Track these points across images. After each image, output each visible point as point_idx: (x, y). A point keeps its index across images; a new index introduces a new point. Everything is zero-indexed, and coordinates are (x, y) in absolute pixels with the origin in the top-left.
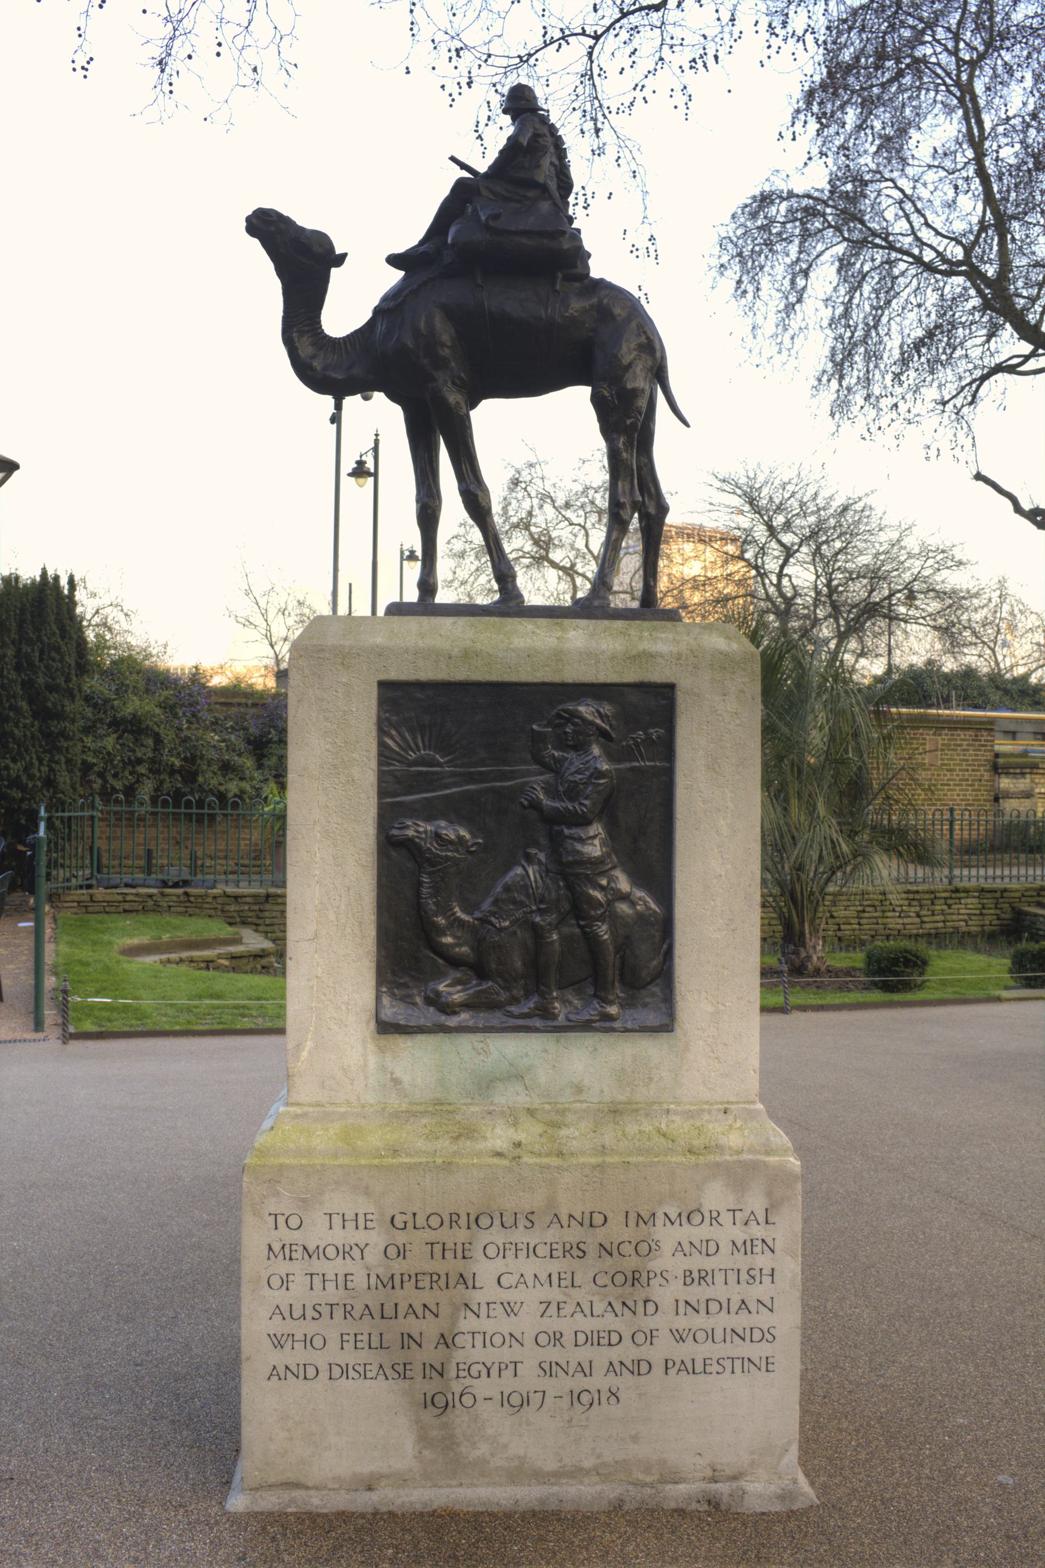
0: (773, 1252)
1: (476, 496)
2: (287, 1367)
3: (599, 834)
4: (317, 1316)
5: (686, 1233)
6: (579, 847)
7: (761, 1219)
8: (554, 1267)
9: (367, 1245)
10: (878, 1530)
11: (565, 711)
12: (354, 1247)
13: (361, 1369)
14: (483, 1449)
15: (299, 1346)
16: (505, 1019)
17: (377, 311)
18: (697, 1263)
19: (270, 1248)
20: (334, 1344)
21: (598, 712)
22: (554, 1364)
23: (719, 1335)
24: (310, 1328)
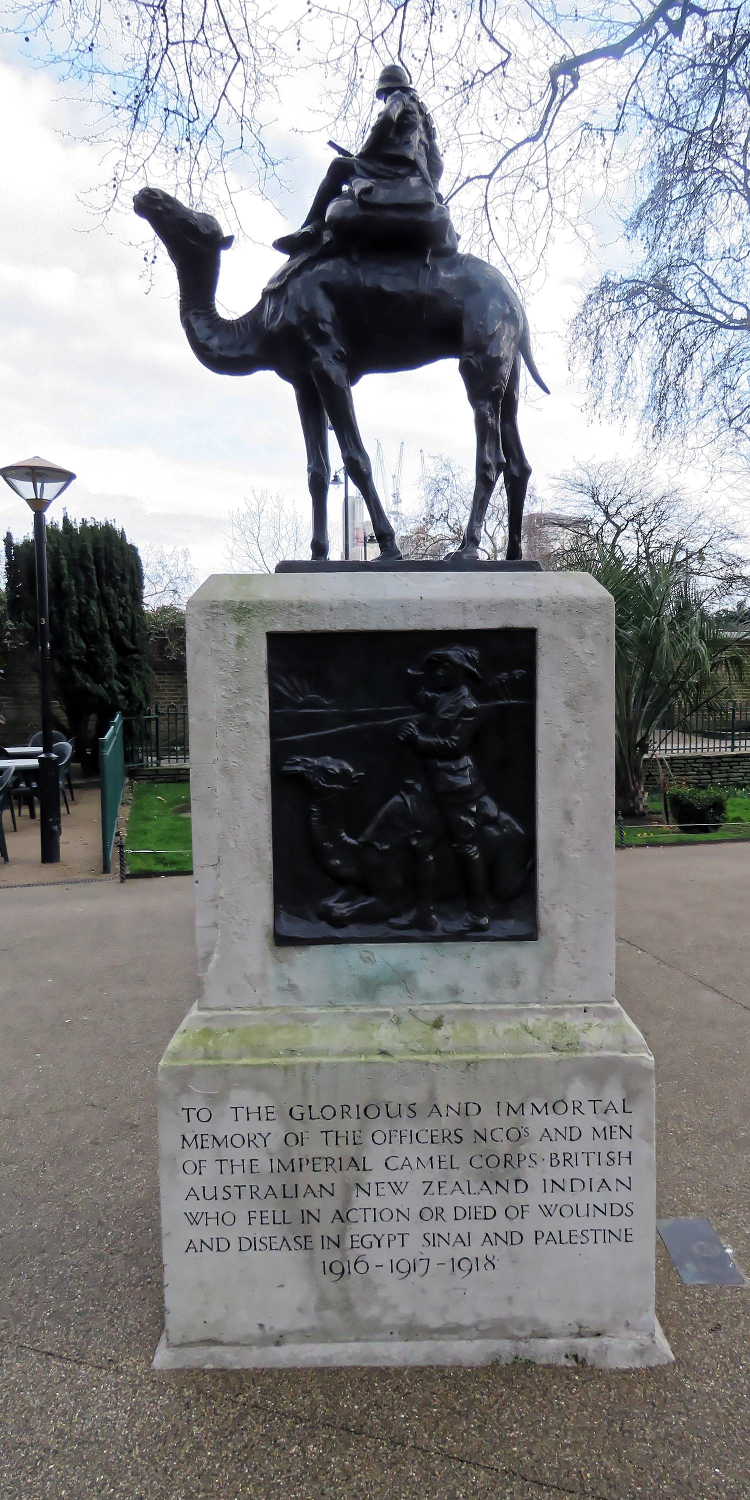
0: (630, 1137)
1: (357, 462)
2: (202, 1241)
3: (469, 765)
4: (227, 1196)
5: (551, 1121)
6: (451, 778)
7: (619, 1108)
8: (433, 1151)
9: (269, 1134)
10: (731, 1397)
11: (435, 655)
12: (258, 1136)
13: (267, 1242)
14: (374, 1311)
15: (212, 1222)
16: (388, 930)
17: (266, 294)
18: (562, 1146)
19: (184, 1139)
20: (243, 1219)
21: (466, 656)
22: (436, 1236)
23: (582, 1210)
24: (219, 1206)
